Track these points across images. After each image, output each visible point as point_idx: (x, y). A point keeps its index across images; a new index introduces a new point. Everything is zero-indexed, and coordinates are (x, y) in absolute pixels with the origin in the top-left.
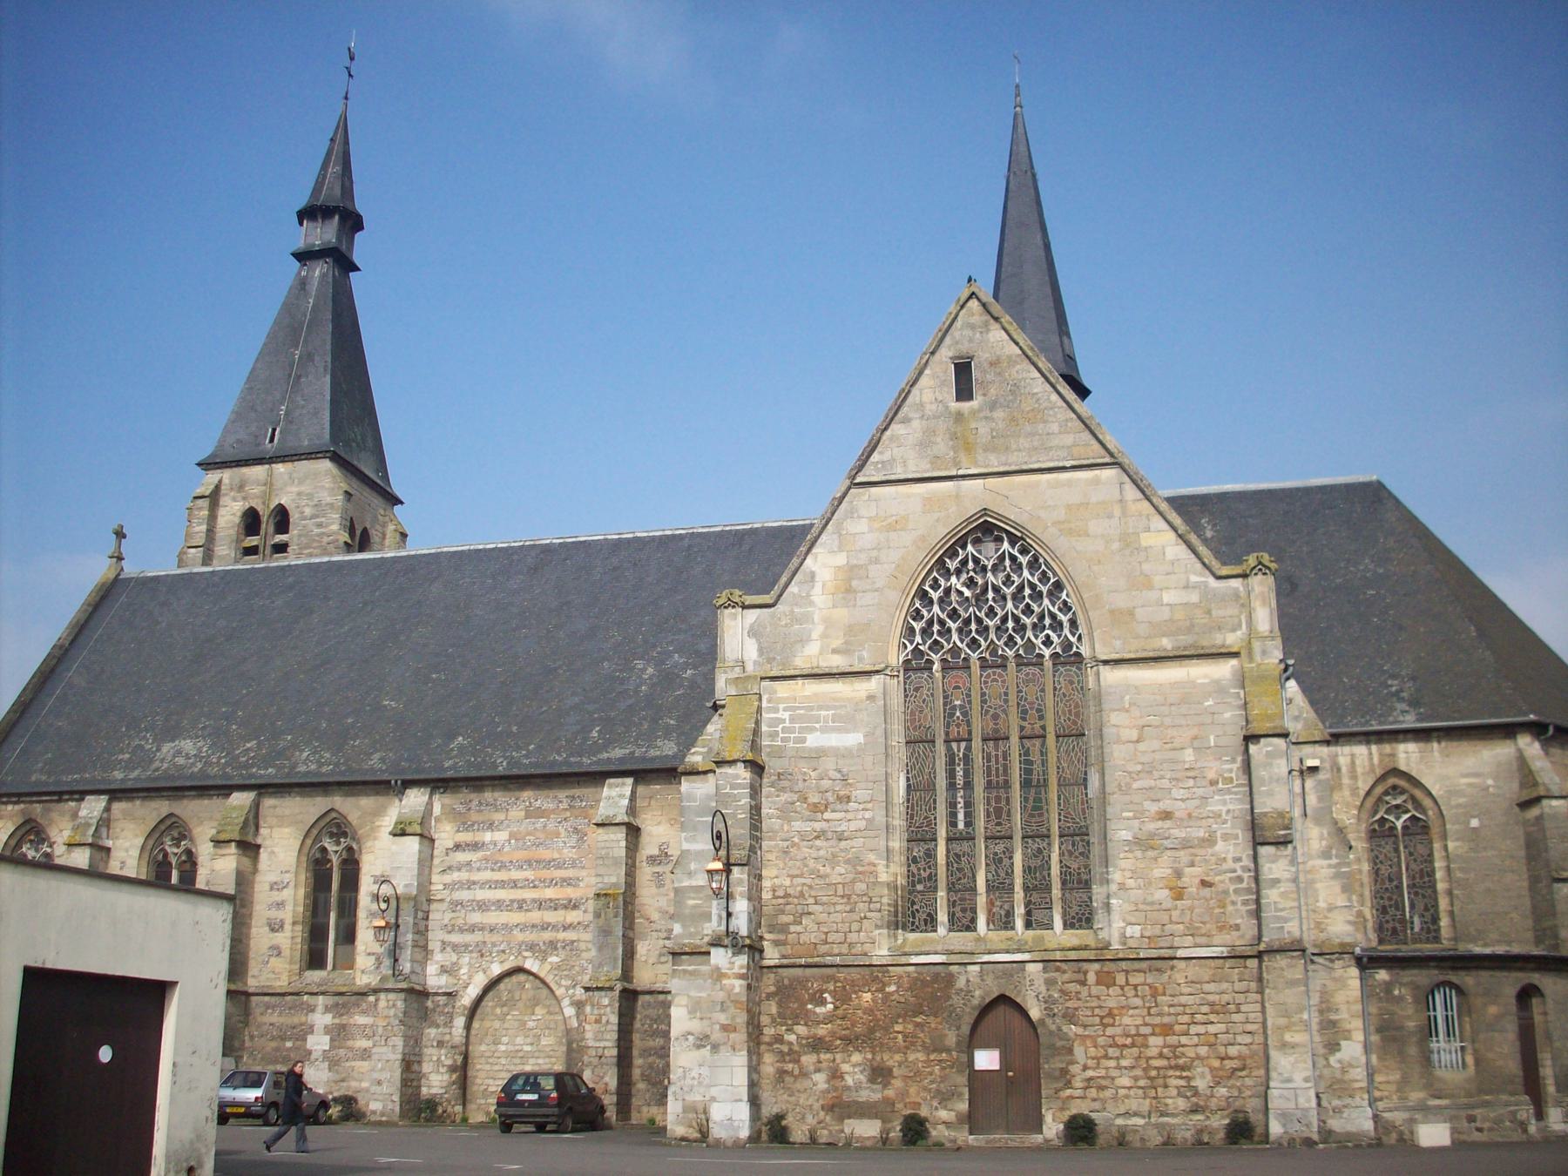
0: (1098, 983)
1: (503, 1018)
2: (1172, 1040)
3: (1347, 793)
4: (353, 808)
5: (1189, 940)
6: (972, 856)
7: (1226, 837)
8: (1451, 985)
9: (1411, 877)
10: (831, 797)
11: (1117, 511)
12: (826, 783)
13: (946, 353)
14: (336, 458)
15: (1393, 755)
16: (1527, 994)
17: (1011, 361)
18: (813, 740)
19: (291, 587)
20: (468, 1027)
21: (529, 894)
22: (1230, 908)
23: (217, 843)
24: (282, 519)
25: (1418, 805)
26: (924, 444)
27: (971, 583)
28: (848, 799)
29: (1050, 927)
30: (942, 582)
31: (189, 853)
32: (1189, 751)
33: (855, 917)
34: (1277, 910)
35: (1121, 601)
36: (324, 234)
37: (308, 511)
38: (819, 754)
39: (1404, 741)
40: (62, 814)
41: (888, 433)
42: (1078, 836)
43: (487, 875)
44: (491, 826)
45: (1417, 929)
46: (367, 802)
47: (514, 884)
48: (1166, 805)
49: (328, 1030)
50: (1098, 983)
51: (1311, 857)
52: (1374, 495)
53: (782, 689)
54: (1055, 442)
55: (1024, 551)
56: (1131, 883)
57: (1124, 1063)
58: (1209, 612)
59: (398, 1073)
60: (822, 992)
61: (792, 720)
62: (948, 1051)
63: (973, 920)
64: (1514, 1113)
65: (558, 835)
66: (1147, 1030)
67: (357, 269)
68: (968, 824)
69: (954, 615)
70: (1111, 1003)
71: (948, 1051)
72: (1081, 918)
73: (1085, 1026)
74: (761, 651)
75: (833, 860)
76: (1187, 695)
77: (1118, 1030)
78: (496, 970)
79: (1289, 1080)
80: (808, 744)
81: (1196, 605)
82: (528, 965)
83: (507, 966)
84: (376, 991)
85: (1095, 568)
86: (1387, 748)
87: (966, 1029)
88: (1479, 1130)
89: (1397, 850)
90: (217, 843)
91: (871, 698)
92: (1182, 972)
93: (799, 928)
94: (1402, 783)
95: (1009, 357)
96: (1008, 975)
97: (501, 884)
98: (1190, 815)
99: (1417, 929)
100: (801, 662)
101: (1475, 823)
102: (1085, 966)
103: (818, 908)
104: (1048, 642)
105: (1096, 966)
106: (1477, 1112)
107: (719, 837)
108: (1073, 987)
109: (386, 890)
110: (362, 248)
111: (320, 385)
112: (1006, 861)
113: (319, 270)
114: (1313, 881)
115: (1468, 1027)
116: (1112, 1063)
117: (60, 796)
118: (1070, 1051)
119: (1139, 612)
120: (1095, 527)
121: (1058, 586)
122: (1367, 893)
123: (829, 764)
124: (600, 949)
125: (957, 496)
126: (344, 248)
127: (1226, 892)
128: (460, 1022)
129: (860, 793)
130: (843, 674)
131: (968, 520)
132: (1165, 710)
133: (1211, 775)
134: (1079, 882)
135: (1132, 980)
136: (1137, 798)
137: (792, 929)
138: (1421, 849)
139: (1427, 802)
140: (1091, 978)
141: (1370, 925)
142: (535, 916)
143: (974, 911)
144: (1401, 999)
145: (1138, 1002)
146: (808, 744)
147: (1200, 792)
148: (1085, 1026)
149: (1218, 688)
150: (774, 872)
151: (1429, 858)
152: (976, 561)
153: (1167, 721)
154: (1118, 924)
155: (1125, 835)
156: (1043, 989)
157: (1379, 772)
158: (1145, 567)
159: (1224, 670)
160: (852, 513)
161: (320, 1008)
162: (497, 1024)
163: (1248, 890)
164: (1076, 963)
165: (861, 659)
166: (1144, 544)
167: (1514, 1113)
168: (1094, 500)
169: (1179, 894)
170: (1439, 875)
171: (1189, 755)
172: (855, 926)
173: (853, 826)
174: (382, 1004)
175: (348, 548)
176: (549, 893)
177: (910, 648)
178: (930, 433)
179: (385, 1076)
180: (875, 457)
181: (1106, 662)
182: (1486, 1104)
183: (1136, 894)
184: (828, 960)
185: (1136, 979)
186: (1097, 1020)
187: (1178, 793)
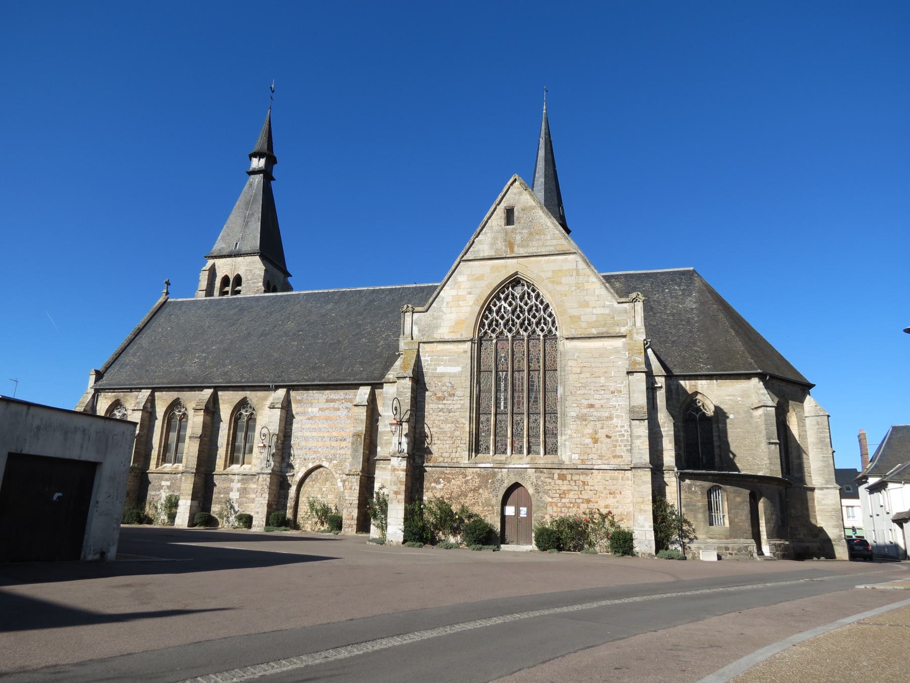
0: (559, 479)
4: (253, 397)
5: (599, 462)
7: (618, 416)
11: (574, 274)
12: (444, 388)
17: (532, 208)
18: (440, 369)
19: (237, 306)
22: (618, 448)
23: (196, 410)
24: (238, 280)
26: (493, 244)
27: (510, 304)
29: (538, 453)
31: (184, 414)
33: (455, 446)
35: (575, 312)
37: (249, 277)
38: (442, 375)
40: (132, 397)
42: (550, 413)
45: (704, 462)
46: (260, 394)
48: (592, 402)
49: (239, 490)
50: (559, 479)
54: (549, 243)
55: (534, 291)
59: (266, 509)
60: (439, 478)
62: (493, 506)
63: (506, 449)
66: (580, 501)
67: (274, 179)
68: (505, 407)
69: (502, 318)
72: (552, 449)
73: (552, 498)
74: (419, 331)
75: (446, 421)
76: (602, 354)
78: (311, 466)
79: (643, 526)
80: (438, 371)
81: (608, 315)
82: (324, 464)
84: (259, 474)
86: (693, 382)
88: (731, 554)
90: (196, 410)
91: (465, 352)
99: (704, 462)
100: (437, 336)
103: (439, 442)
104: (542, 330)
105: (558, 471)
106: (729, 546)
107: (396, 409)
108: (548, 480)
109: (265, 431)
110: (276, 171)
117: (131, 390)
119: (583, 318)
120: (564, 280)
121: (547, 306)
122: (682, 445)
123: (446, 380)
124: (353, 458)
127: (617, 441)
130: (454, 341)
133: (612, 389)
134: (550, 434)
135: (574, 478)
140: (556, 476)
141: (683, 459)
143: (506, 445)
144: (695, 492)
145: (576, 488)
146: (438, 371)
147: (607, 396)
148: (552, 498)
149: (616, 351)
152: (513, 295)
155: (573, 414)
156: (535, 480)
158: (586, 298)
159: (619, 343)
160: (461, 273)
161: (236, 481)
162: (310, 489)
163: (627, 441)
167: (747, 547)
168: (564, 268)
169: (596, 441)
170: (715, 439)
172: (454, 450)
174: (261, 479)
175: (265, 292)
178: (495, 238)
179: (260, 510)
184: (442, 464)
185: (576, 477)
187: (597, 397)
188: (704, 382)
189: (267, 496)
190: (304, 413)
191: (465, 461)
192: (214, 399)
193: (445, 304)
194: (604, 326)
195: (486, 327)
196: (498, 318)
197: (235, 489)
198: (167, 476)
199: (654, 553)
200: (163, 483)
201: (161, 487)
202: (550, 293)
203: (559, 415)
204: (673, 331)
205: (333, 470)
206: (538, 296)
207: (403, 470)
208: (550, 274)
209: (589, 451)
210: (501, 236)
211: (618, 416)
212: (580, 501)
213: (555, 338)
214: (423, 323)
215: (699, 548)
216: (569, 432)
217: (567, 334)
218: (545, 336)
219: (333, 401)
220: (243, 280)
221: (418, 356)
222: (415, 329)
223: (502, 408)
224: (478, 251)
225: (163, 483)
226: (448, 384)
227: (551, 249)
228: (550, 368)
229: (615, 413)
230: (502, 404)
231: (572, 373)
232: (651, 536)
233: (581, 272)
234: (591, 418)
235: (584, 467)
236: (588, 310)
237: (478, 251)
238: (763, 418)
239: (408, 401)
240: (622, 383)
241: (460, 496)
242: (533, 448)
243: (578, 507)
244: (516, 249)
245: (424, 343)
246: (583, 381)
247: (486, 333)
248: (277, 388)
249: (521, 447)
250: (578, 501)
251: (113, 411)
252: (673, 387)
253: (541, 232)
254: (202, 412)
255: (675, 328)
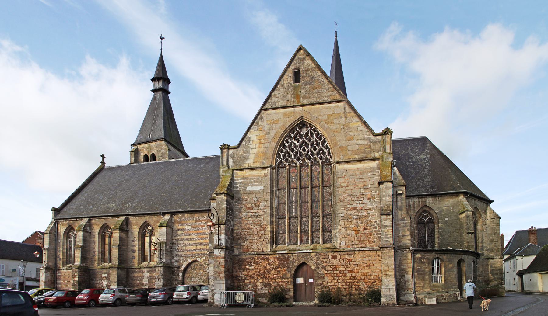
1: (192, 273)
2: (354, 274)
3: (412, 212)
5: (360, 246)
6: (296, 223)
7: (372, 215)
8: (439, 258)
9: (428, 234)
10: (253, 205)
11: (343, 116)
12: (253, 201)
13: (292, 67)
14: (165, 140)
15: (425, 202)
16: (460, 262)
17: (312, 70)
18: (249, 189)
20: (183, 276)
21: (197, 242)
22: (372, 236)
25: (430, 214)
26: (284, 97)
27: (298, 141)
28: (259, 206)
30: (289, 140)
32: (362, 189)
34: (386, 235)
35: (343, 144)
36: (160, 84)
38: (251, 192)
39: (429, 197)
41: (273, 94)
43: (186, 237)
44: (187, 225)
47: (193, 239)
48: (355, 206)
49: (148, 277)
51: (398, 221)
52: (425, 140)
53: (239, 173)
55: (315, 131)
56: (343, 229)
57: (339, 281)
58: (370, 147)
61: (242, 183)
63: (297, 241)
64: (455, 294)
65: (204, 226)
66: (347, 272)
68: (296, 213)
70: (336, 264)
71: (288, 279)
74: (234, 162)
75: (254, 224)
76: (363, 172)
77: (338, 272)
78: (190, 261)
81: (367, 145)
82: (197, 260)
83: (192, 260)
85: (336, 134)
87: (293, 272)
89: (425, 227)
91: (266, 175)
92: (358, 255)
93: (244, 244)
94: (427, 209)
95: (312, 68)
96: (305, 256)
97: (190, 239)
98: (362, 209)
101: (446, 219)
102: (328, 254)
103: (250, 238)
104: (321, 158)
105: (332, 254)
108: (325, 260)
110: (171, 88)
111: (161, 123)
112: (307, 224)
113: (160, 94)
114: (398, 228)
115: (443, 270)
116: (336, 281)
118: (324, 278)
119: (349, 148)
120: (336, 121)
121: (324, 141)
125: (294, 112)
126: (165, 88)
128: (181, 274)
129: (262, 204)
131: (297, 120)
132: (355, 177)
133: (369, 196)
135: (342, 257)
136: (346, 204)
137: (242, 244)
138: (431, 227)
139: (434, 214)
140: (330, 257)
142: (199, 247)
144: (424, 262)
147: (364, 201)
148: (328, 271)
149: (372, 170)
150: (237, 228)
151: (434, 229)
152: (300, 134)
153: (356, 180)
154: (339, 241)
155: (342, 215)
157: (421, 206)
158: (351, 133)
159: (374, 164)
161: (146, 272)
162: (191, 275)
164: (326, 251)
165: (263, 164)
166: (351, 126)
169: (357, 232)
171: (362, 190)
172: (261, 243)
173: (260, 214)
174: (157, 270)
176: (202, 241)
177: (279, 161)
178: (286, 93)
180: (269, 101)
181: (338, 163)
182: (447, 292)
183: (344, 232)
186: (331, 269)
187: (357, 202)
188: (430, 199)
189: (162, 280)
190: (183, 230)
191: (268, 250)
192: (127, 222)
193: (251, 142)
194: (364, 153)
195: (282, 158)
196: (289, 151)
197: (146, 277)
198: (105, 271)
199: (396, 303)
200: (103, 275)
201: (102, 278)
202: (326, 131)
203: (332, 217)
204: (412, 171)
205: (203, 263)
206: (318, 134)
207: (222, 258)
208: (325, 117)
209: (353, 239)
210: (290, 91)
211: (372, 215)
212: (347, 272)
213: (330, 163)
214: (236, 156)
215: (425, 297)
216: (339, 227)
217: (337, 159)
218: (323, 162)
219: (200, 221)
220: (157, 156)
221: (232, 179)
222: (231, 161)
223: (294, 214)
224: (274, 102)
225: (103, 275)
226: (255, 199)
227: (326, 99)
228: (327, 186)
229: (370, 213)
230: (294, 211)
231: (341, 187)
232: (394, 292)
233: (348, 114)
234: (354, 217)
235: (349, 249)
236: (353, 142)
237: (274, 102)
238: (465, 219)
239: (224, 210)
240: (376, 192)
241: (265, 273)
242: (316, 239)
243: (346, 276)
244: (301, 99)
245: (237, 170)
246: (349, 192)
247: (281, 162)
248: (164, 214)
249: (307, 239)
250: (345, 272)
251: (69, 233)
252: (411, 203)
253: (320, 86)
254: (118, 231)
255: (414, 169)
